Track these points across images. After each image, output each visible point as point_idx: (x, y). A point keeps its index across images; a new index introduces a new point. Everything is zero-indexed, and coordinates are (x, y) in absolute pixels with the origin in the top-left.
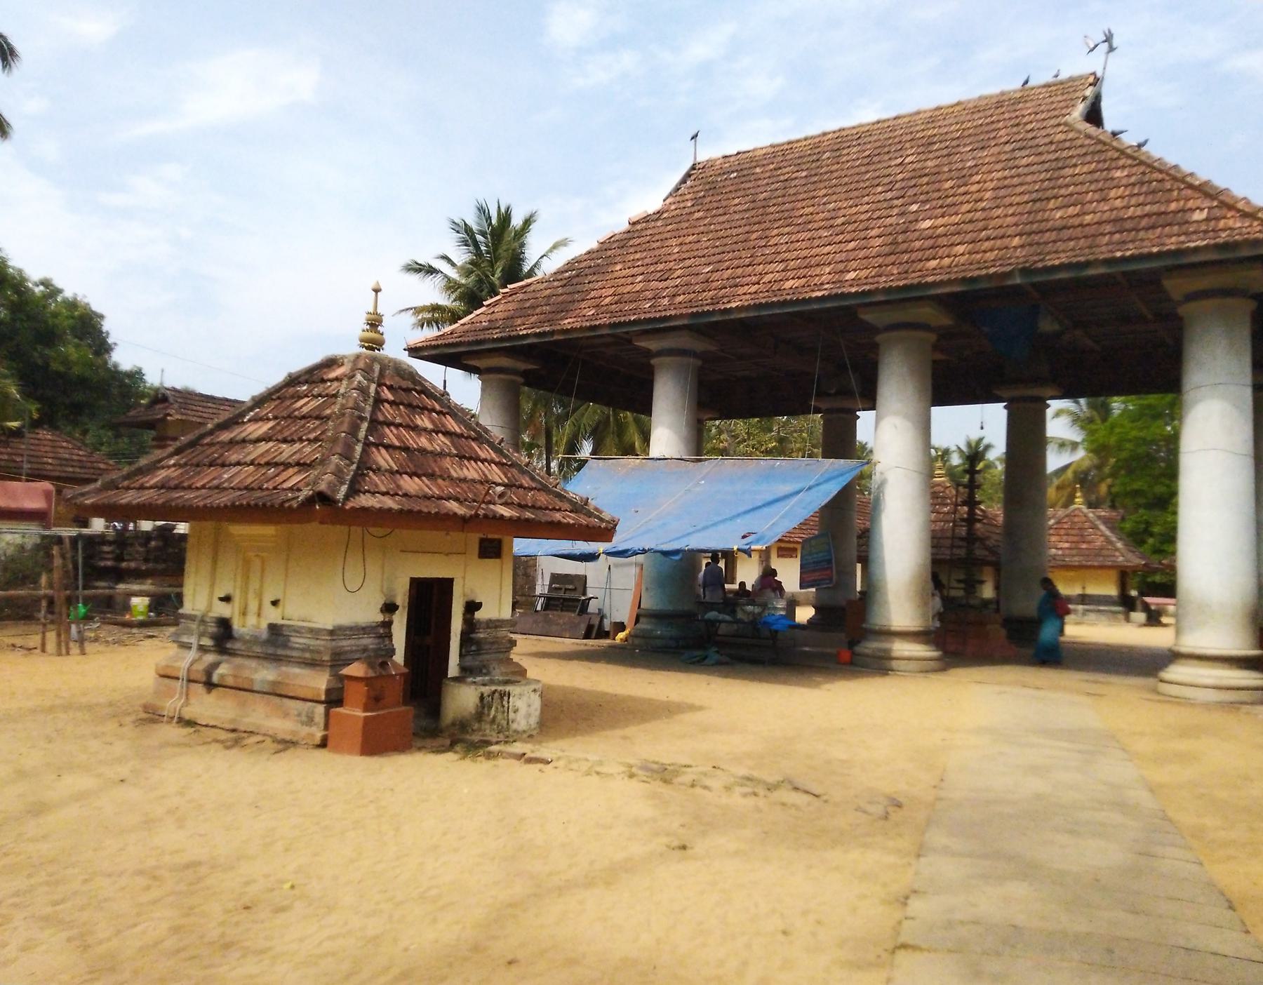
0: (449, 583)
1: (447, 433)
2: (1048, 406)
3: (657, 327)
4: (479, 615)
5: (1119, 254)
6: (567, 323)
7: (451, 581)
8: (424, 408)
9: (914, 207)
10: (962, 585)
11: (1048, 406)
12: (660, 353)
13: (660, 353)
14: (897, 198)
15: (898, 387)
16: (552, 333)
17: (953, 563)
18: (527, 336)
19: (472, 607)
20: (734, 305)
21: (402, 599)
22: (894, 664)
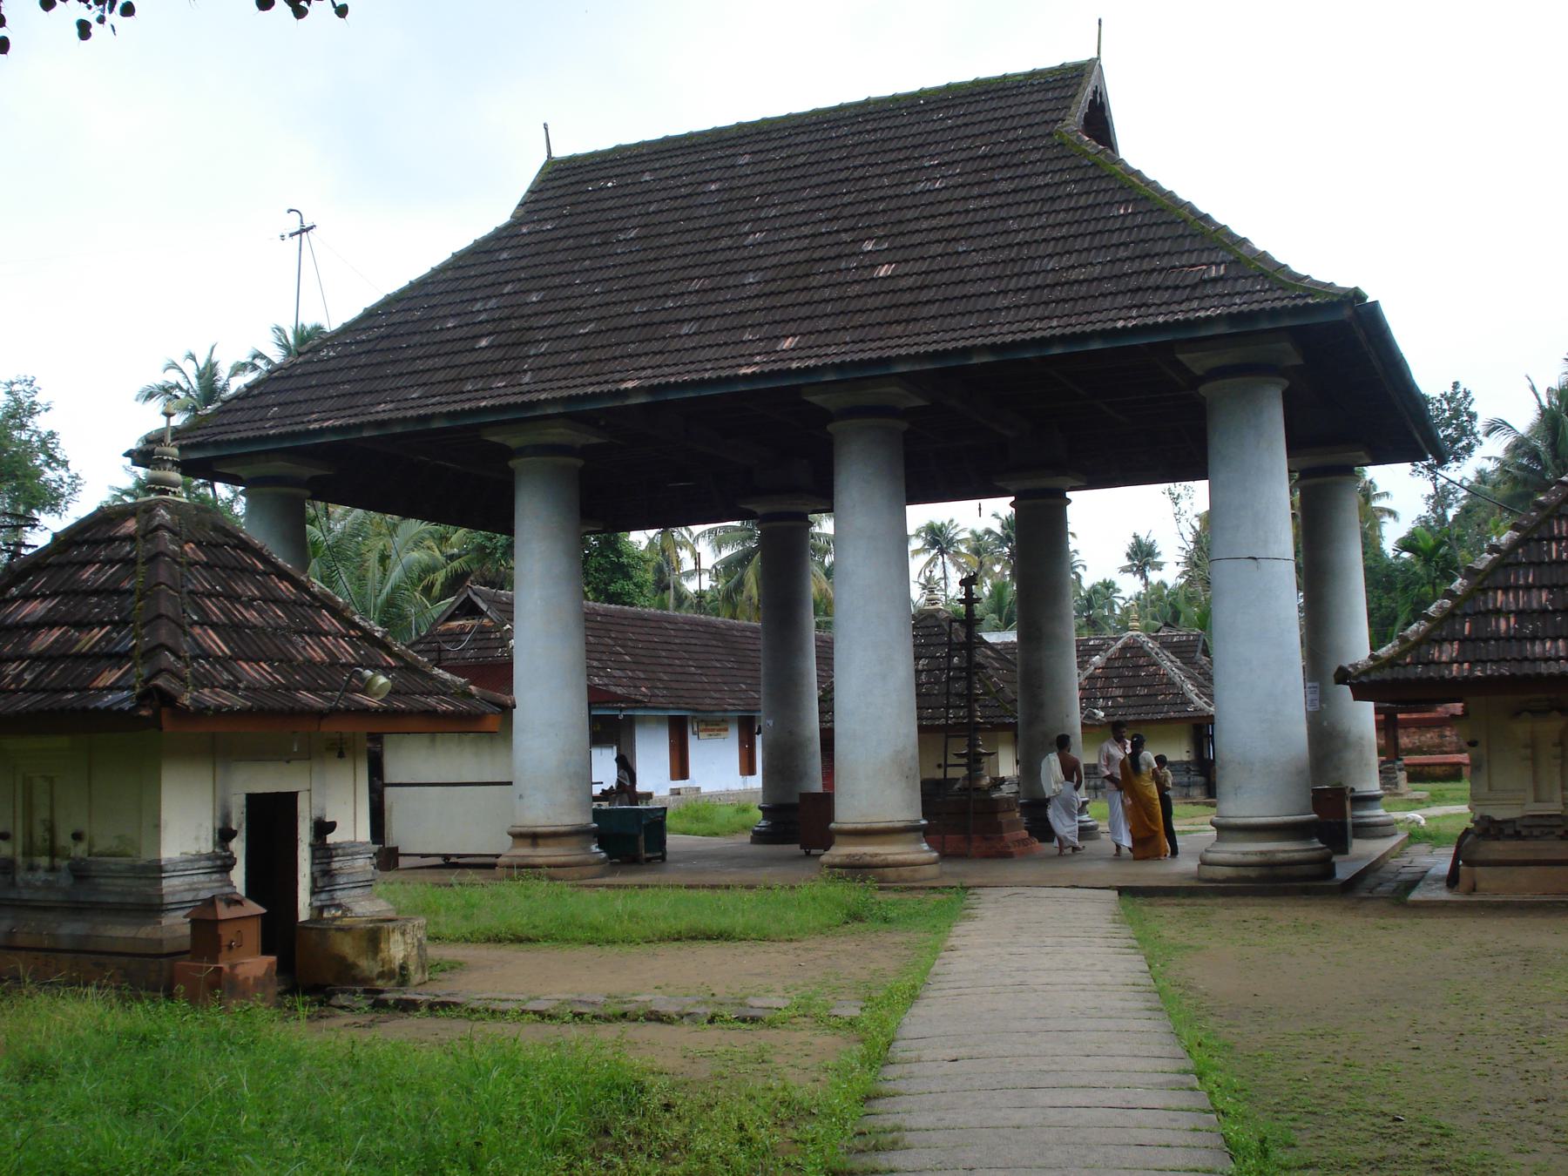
0: (291, 799)
1: (277, 601)
2: (1069, 501)
3: (522, 415)
4: (331, 838)
5: (1120, 324)
6: (384, 410)
7: (252, 799)
8: (244, 570)
9: (869, 246)
10: (964, 761)
11: (1069, 501)
12: (520, 452)
13: (520, 452)
14: (846, 231)
15: (858, 484)
16: (360, 427)
17: (949, 731)
18: (322, 431)
19: (323, 828)
20: (630, 385)
21: (238, 820)
22: (909, 1138)
